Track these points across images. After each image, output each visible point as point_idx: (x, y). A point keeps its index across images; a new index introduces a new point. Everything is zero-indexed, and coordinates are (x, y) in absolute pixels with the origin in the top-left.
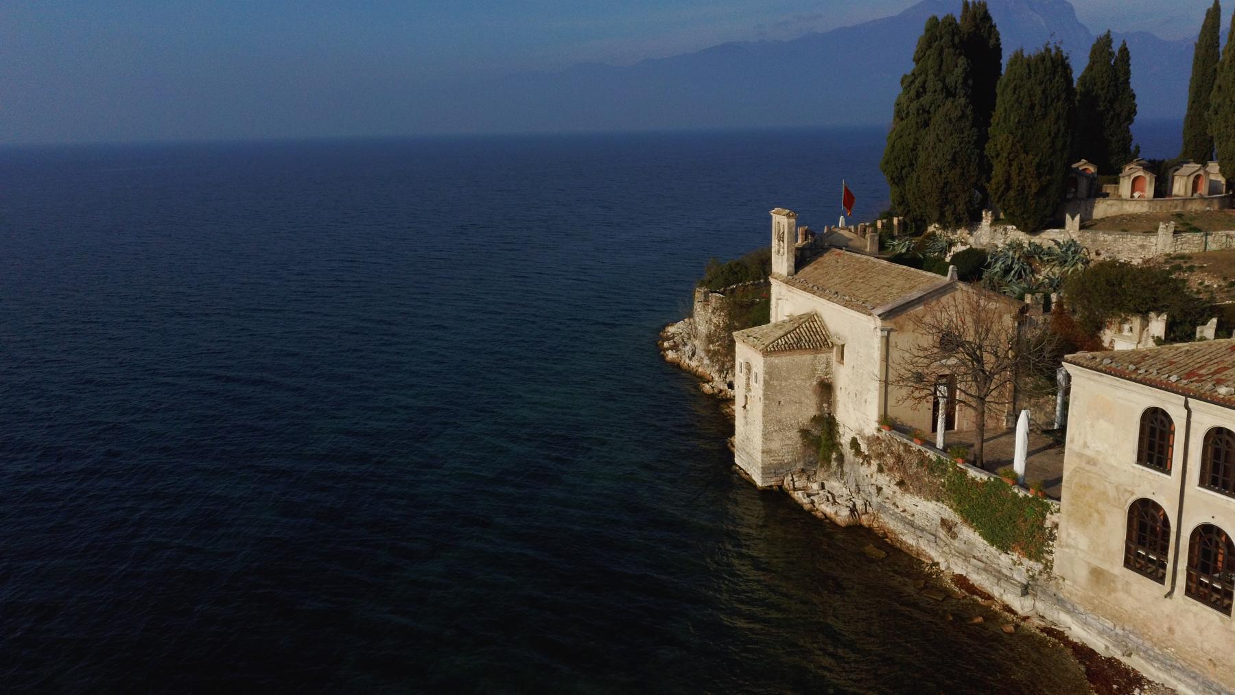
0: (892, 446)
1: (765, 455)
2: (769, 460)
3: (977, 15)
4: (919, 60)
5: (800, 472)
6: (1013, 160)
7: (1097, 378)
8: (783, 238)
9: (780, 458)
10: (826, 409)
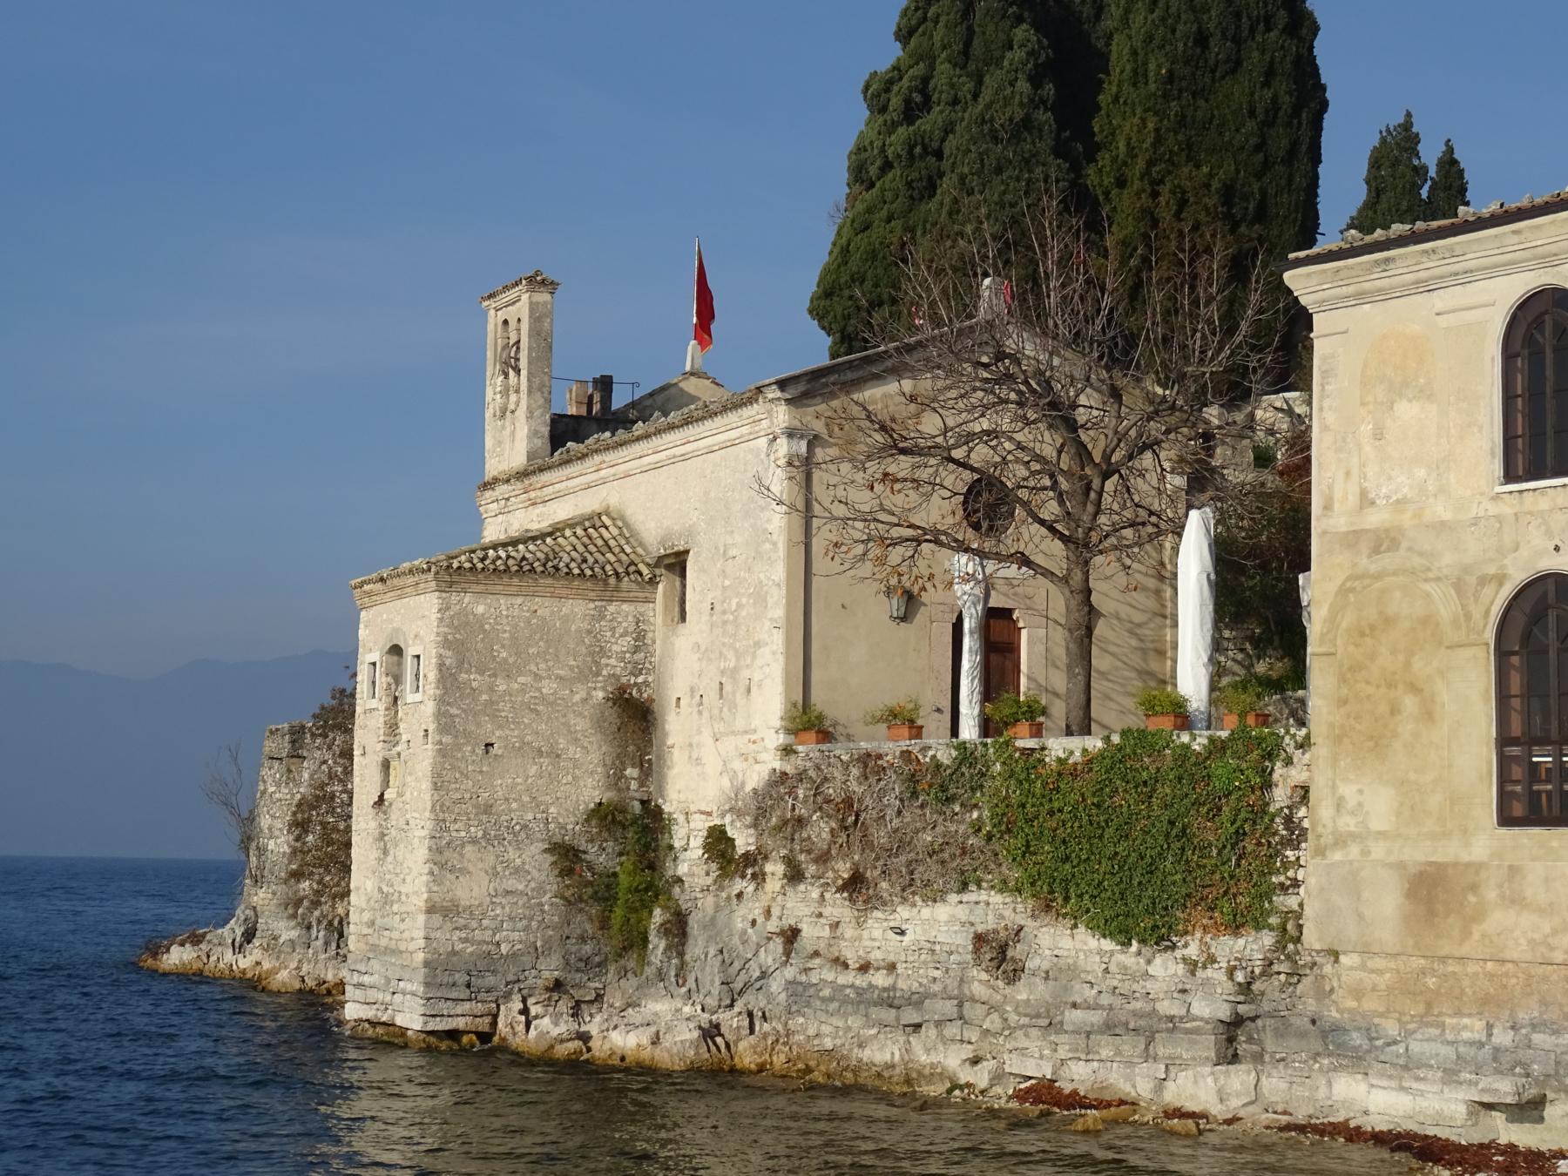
0: (826, 779)
1: (437, 919)
2: (449, 938)
4: (911, 33)
5: (547, 989)
6: (1161, 182)
8: (517, 360)
9: (487, 935)
10: (634, 785)
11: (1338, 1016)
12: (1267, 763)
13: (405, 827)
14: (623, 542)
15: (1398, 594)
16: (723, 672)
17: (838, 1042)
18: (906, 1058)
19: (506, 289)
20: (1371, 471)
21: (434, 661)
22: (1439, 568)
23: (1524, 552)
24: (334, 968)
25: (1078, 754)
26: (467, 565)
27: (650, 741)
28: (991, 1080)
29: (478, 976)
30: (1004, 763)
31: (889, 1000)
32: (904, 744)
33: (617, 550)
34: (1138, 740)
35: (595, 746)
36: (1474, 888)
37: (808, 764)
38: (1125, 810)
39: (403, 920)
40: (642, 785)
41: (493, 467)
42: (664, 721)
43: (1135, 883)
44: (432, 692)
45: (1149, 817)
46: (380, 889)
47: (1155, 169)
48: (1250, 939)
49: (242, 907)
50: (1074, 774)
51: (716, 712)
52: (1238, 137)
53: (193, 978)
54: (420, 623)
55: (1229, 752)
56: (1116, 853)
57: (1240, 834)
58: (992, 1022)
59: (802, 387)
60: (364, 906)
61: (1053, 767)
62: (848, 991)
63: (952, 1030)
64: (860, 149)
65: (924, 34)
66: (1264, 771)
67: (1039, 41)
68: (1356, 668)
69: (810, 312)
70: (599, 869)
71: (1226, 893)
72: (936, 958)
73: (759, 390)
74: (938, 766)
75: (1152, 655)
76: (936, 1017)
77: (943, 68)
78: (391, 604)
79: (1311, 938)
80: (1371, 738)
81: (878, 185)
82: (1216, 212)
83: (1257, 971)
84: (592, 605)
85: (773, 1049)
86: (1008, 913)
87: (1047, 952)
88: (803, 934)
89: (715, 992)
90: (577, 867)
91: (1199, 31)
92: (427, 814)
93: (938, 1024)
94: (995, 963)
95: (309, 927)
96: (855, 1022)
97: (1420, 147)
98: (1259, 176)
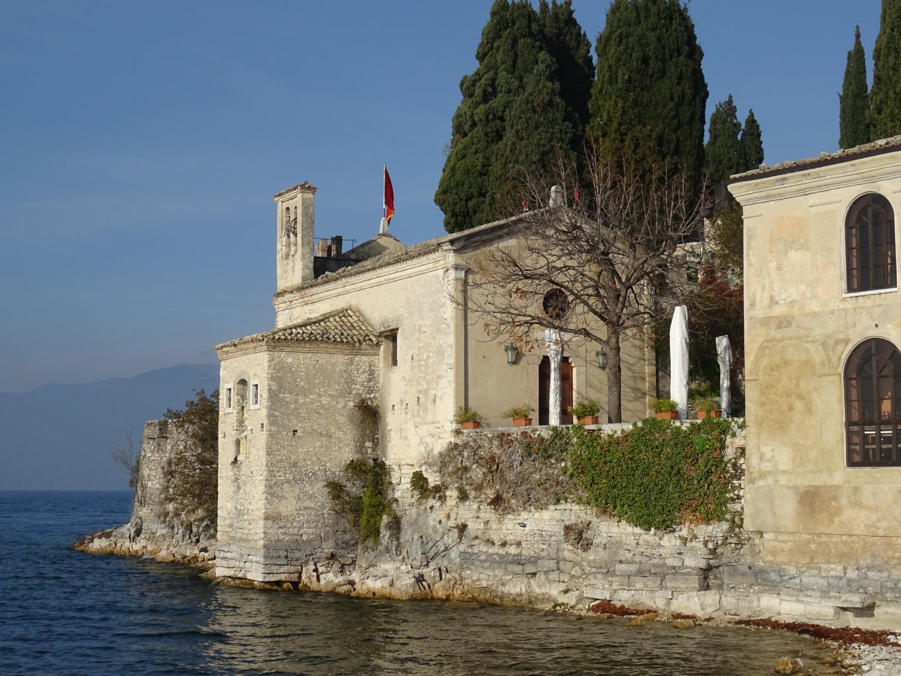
0: (480, 447)
1: (270, 523)
2: (277, 533)
3: (560, 16)
4: (484, 55)
5: (327, 558)
6: (626, 134)
7: (779, 189)
9: (296, 531)
10: (370, 451)
11: (763, 565)
12: (722, 436)
13: (251, 475)
14: (360, 324)
15: (791, 349)
16: (419, 392)
17: (490, 583)
18: (529, 590)
19: (289, 191)
20: (776, 287)
21: (266, 387)
22: (813, 336)
23: (859, 328)
24: (190, 548)
25: (619, 432)
26: (283, 337)
27: (378, 427)
28: (577, 601)
29: (291, 553)
30: (579, 438)
31: (518, 561)
32: (523, 428)
33: (358, 328)
34: (652, 423)
35: (350, 431)
36: (835, 498)
37: (470, 439)
38: (646, 461)
39: (250, 524)
40: (374, 450)
41: (281, 285)
42: (385, 417)
43: (653, 498)
44: (265, 404)
45: (659, 464)
46: (236, 508)
47: (622, 128)
48: (716, 526)
49: (134, 517)
50: (618, 442)
51: (416, 412)
52: (665, 110)
53: (109, 556)
54: (257, 368)
55: (702, 431)
56: (642, 483)
57: (709, 473)
58: (576, 571)
59: (462, 243)
60: (226, 516)
61: (606, 439)
62: (495, 556)
63: (553, 576)
64: (458, 116)
65: (491, 56)
66: (721, 440)
67: (551, 60)
68: (769, 387)
69: (435, 201)
70: (353, 495)
71: (702, 503)
72: (543, 539)
73: (439, 245)
74: (543, 439)
75: (639, 380)
76: (545, 569)
77: (502, 74)
78: (240, 358)
79: (748, 525)
80: (779, 422)
81: (470, 135)
82: (655, 150)
83: (720, 542)
84: (347, 357)
85: (454, 587)
86: (582, 515)
87: (605, 534)
88: (469, 527)
89: (419, 558)
90: (342, 494)
91: (644, 56)
92: (264, 468)
93: (546, 573)
94: (576, 541)
95: (173, 528)
96: (499, 572)
97: (737, 114)
98: (675, 131)
